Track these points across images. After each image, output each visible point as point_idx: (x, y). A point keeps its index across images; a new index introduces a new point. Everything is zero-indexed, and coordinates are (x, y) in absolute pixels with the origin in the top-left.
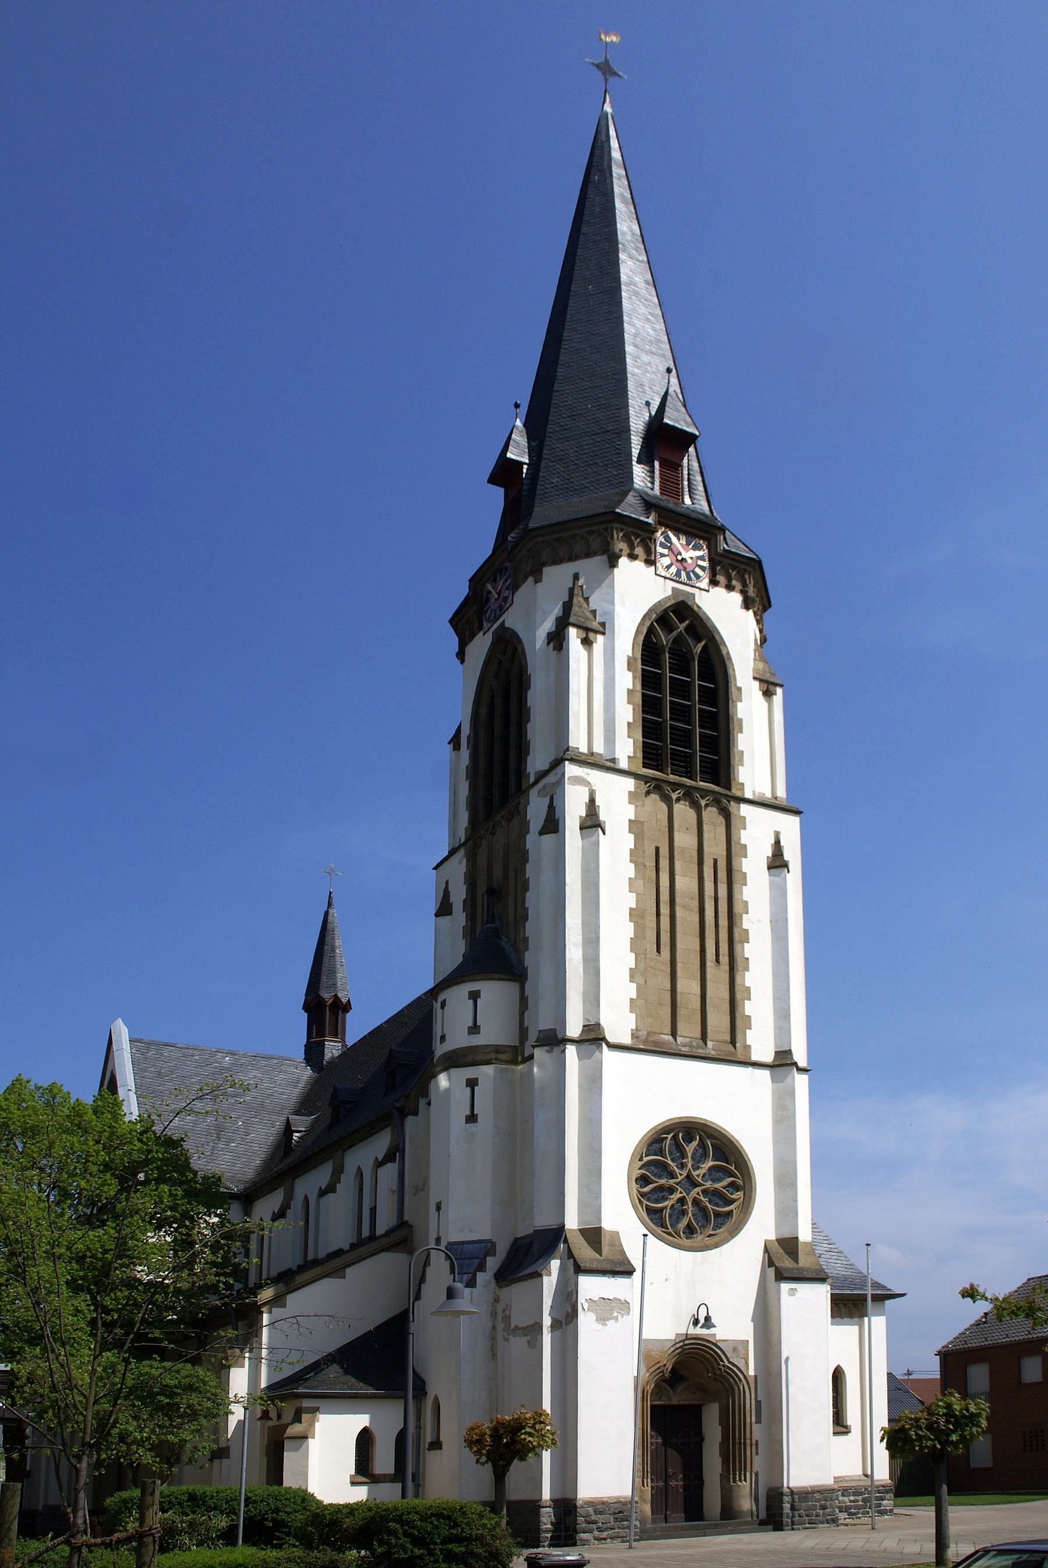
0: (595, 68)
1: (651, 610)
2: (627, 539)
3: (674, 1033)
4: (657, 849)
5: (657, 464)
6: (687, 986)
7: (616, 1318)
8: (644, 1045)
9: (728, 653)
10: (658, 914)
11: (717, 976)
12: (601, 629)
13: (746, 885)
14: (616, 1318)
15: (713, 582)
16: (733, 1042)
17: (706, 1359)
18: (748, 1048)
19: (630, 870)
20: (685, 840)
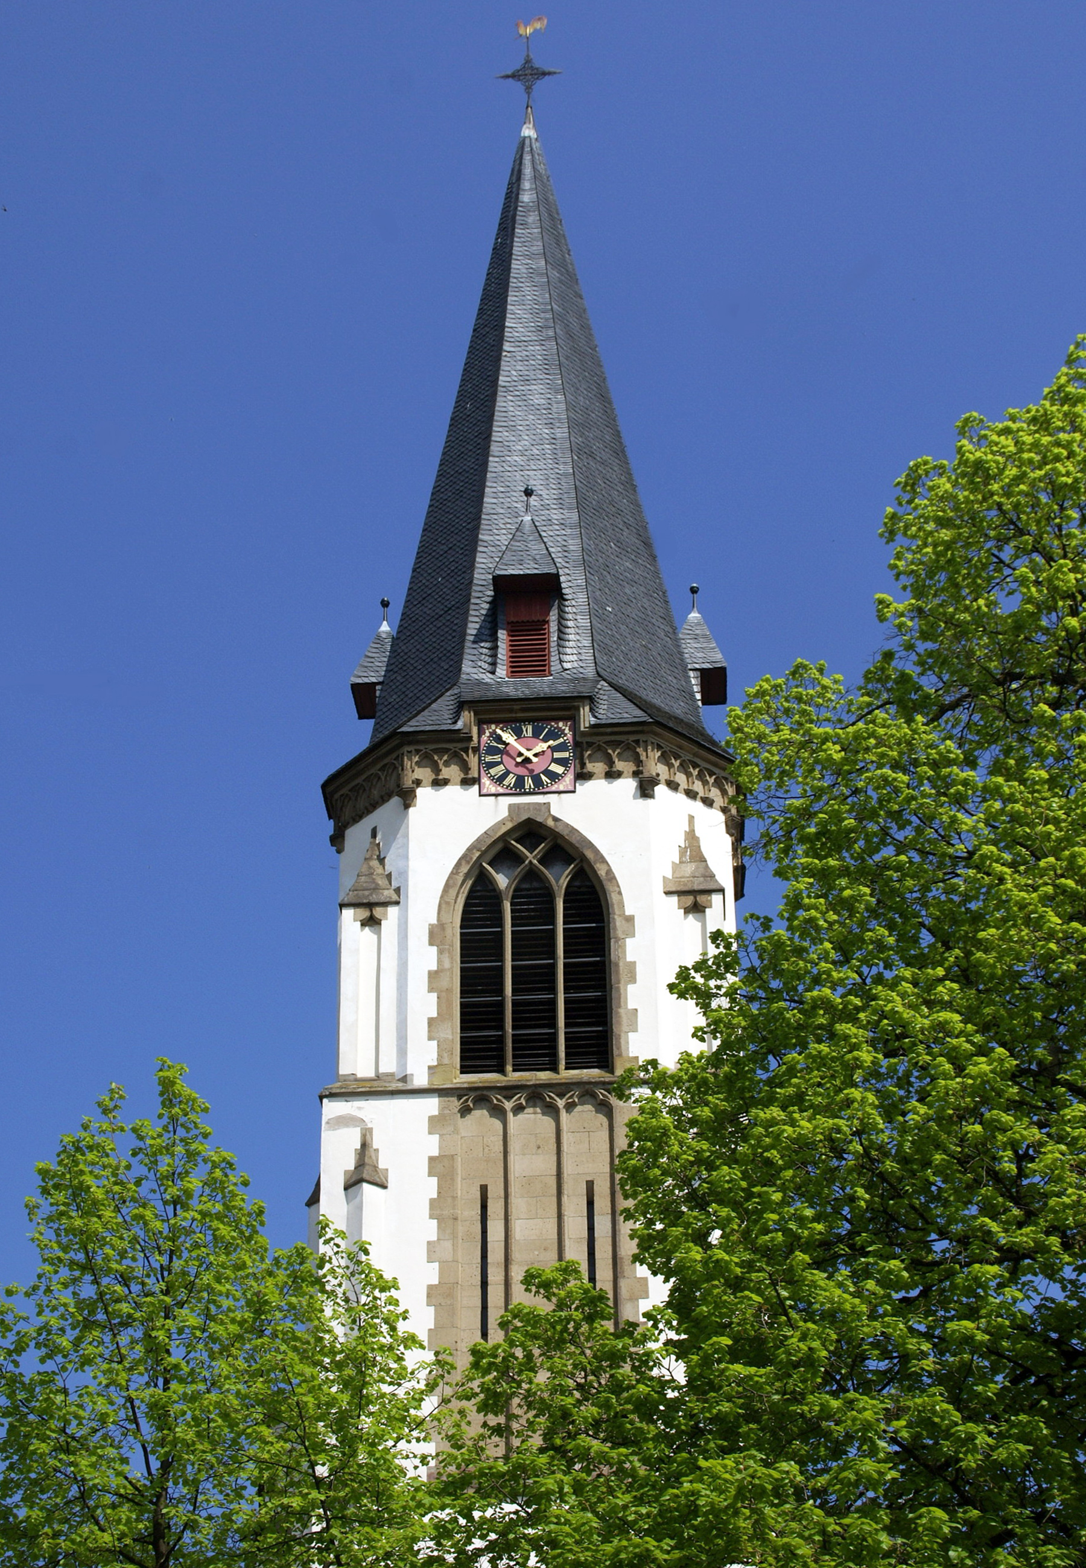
0: (547, 70)
1: (470, 850)
2: (427, 760)
4: (484, 1189)
5: (502, 634)
9: (609, 871)
10: (484, 1284)
12: (395, 897)
15: (583, 776)
19: (430, 1230)
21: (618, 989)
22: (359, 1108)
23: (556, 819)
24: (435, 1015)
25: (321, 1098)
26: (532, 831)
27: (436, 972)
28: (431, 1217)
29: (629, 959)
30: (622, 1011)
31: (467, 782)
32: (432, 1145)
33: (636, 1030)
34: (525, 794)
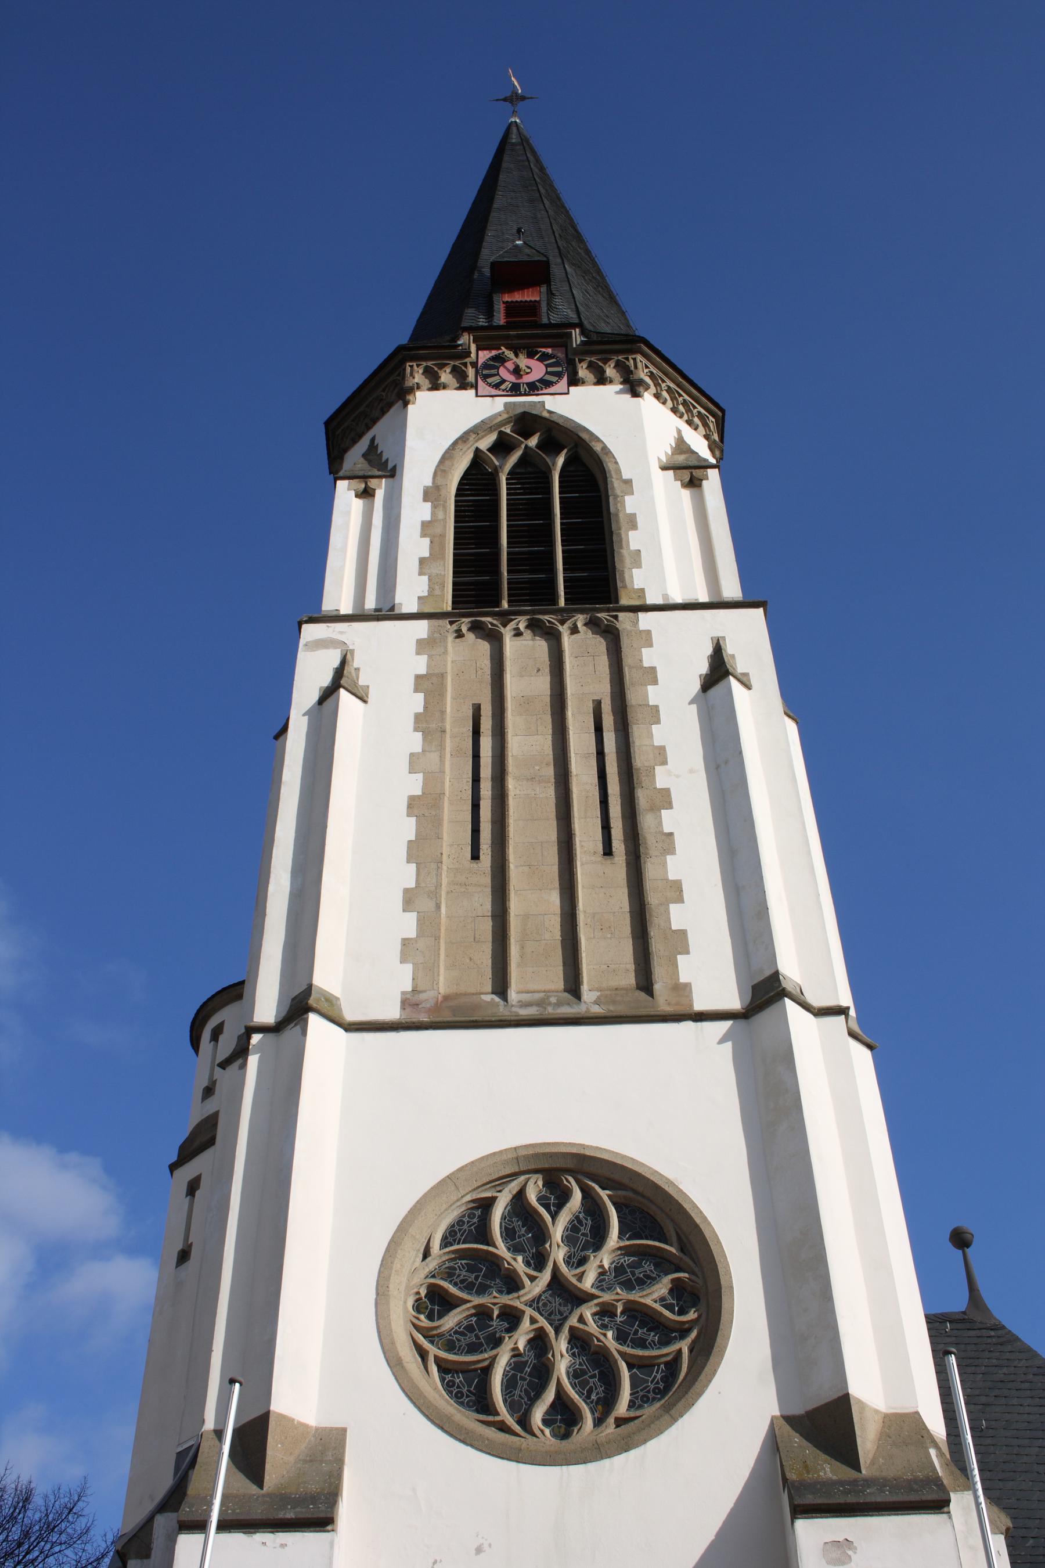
6: (534, 902)
11: (601, 886)
13: (658, 722)
16: (645, 983)
18: (683, 990)
21: (619, 535)
22: (341, 633)
23: (550, 412)
24: (427, 555)
25: (300, 624)
26: (527, 422)
27: (429, 522)
28: (416, 729)
29: (629, 510)
30: (624, 552)
31: (463, 386)
32: (420, 665)
33: (639, 566)
34: (521, 395)
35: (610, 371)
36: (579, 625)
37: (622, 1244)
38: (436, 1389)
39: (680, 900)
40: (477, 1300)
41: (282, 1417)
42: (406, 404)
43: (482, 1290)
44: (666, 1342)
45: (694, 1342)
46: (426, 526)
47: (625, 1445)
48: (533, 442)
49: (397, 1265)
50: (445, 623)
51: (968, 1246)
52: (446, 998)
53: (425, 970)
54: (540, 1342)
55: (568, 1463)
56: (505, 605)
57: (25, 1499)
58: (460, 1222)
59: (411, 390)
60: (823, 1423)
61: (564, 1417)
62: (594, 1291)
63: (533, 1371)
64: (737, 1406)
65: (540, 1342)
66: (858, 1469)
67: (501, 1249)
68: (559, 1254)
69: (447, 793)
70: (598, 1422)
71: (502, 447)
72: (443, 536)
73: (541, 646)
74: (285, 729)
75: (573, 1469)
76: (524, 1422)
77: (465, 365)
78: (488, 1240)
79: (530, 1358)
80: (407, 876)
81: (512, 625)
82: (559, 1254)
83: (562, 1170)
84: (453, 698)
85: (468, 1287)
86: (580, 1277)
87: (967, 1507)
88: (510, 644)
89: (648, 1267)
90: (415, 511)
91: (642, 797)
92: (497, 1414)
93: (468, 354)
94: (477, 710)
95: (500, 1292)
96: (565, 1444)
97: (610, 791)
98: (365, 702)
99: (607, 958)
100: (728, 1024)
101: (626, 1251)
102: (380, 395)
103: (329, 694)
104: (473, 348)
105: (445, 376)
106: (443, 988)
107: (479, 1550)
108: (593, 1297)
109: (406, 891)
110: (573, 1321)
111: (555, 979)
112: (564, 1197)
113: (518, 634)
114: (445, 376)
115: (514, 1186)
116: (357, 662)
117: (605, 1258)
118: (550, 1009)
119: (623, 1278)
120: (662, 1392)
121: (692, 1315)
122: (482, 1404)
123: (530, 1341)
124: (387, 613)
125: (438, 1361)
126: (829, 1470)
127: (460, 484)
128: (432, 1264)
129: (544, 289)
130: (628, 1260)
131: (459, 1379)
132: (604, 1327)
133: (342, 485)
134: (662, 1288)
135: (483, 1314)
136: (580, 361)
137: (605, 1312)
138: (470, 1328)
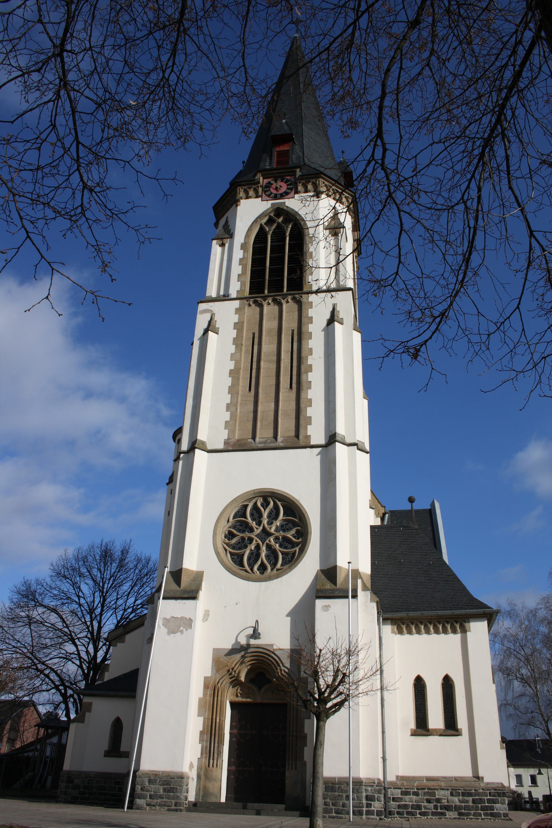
3: (254, 438)
6: (266, 406)
7: (182, 632)
8: (234, 446)
11: (287, 398)
13: (311, 339)
14: (182, 632)
16: (297, 436)
17: (266, 662)
18: (308, 437)
20: (270, 324)
23: (287, 207)
24: (240, 273)
26: (279, 211)
28: (233, 344)
31: (257, 197)
32: (236, 318)
34: (277, 199)
35: (310, 187)
36: (289, 300)
37: (285, 518)
38: (228, 560)
39: (311, 406)
40: (241, 535)
41: (186, 569)
42: (237, 206)
43: (243, 532)
44: (293, 547)
45: (300, 547)
46: (241, 260)
47: (277, 577)
48: (280, 220)
49: (219, 525)
50: (245, 301)
51: (413, 502)
52: (238, 440)
53: (232, 432)
54: (258, 547)
55: (261, 581)
56: (266, 292)
57: (148, 561)
58: (238, 511)
59: (239, 201)
60: (329, 572)
61: (263, 568)
62: (274, 532)
63: (255, 556)
64: (309, 566)
65: (258, 547)
66: (336, 585)
67: (249, 520)
68: (265, 521)
69: (242, 368)
70: (272, 570)
71: (270, 221)
72: (246, 264)
73: (276, 308)
74: (192, 344)
75: (263, 583)
76: (252, 569)
77: (258, 187)
78: (246, 518)
79: (255, 552)
80: (227, 399)
81: (267, 301)
82: (265, 521)
83: (268, 496)
84: (247, 331)
85: (239, 531)
86: (270, 528)
87: (364, 596)
88: (266, 308)
89: (290, 525)
90: (238, 254)
91: (303, 368)
92: (244, 567)
93: (259, 183)
94: (254, 334)
95: (248, 532)
96: (263, 576)
97: (294, 365)
98: (218, 334)
99: (286, 426)
100: (320, 449)
101: (284, 520)
102: (225, 205)
103: (206, 331)
104: (261, 178)
105: (251, 193)
106: (237, 437)
107: (237, 604)
108: (273, 534)
109: (227, 404)
110: (267, 541)
111: (270, 433)
112: (268, 504)
113: (269, 304)
114: (251, 193)
115: (254, 501)
116: (216, 318)
117: (278, 523)
118: (268, 444)
119: (283, 528)
120: (290, 561)
121: (300, 540)
122: (241, 564)
123: (255, 547)
124: (226, 298)
125: (230, 552)
126: (329, 586)
127: (255, 238)
128: (230, 524)
129: (291, 144)
130: (284, 523)
131: (236, 557)
132: (276, 543)
133: (214, 242)
134: (293, 532)
135: (243, 539)
136: (300, 183)
137: (277, 539)
138: (239, 543)
